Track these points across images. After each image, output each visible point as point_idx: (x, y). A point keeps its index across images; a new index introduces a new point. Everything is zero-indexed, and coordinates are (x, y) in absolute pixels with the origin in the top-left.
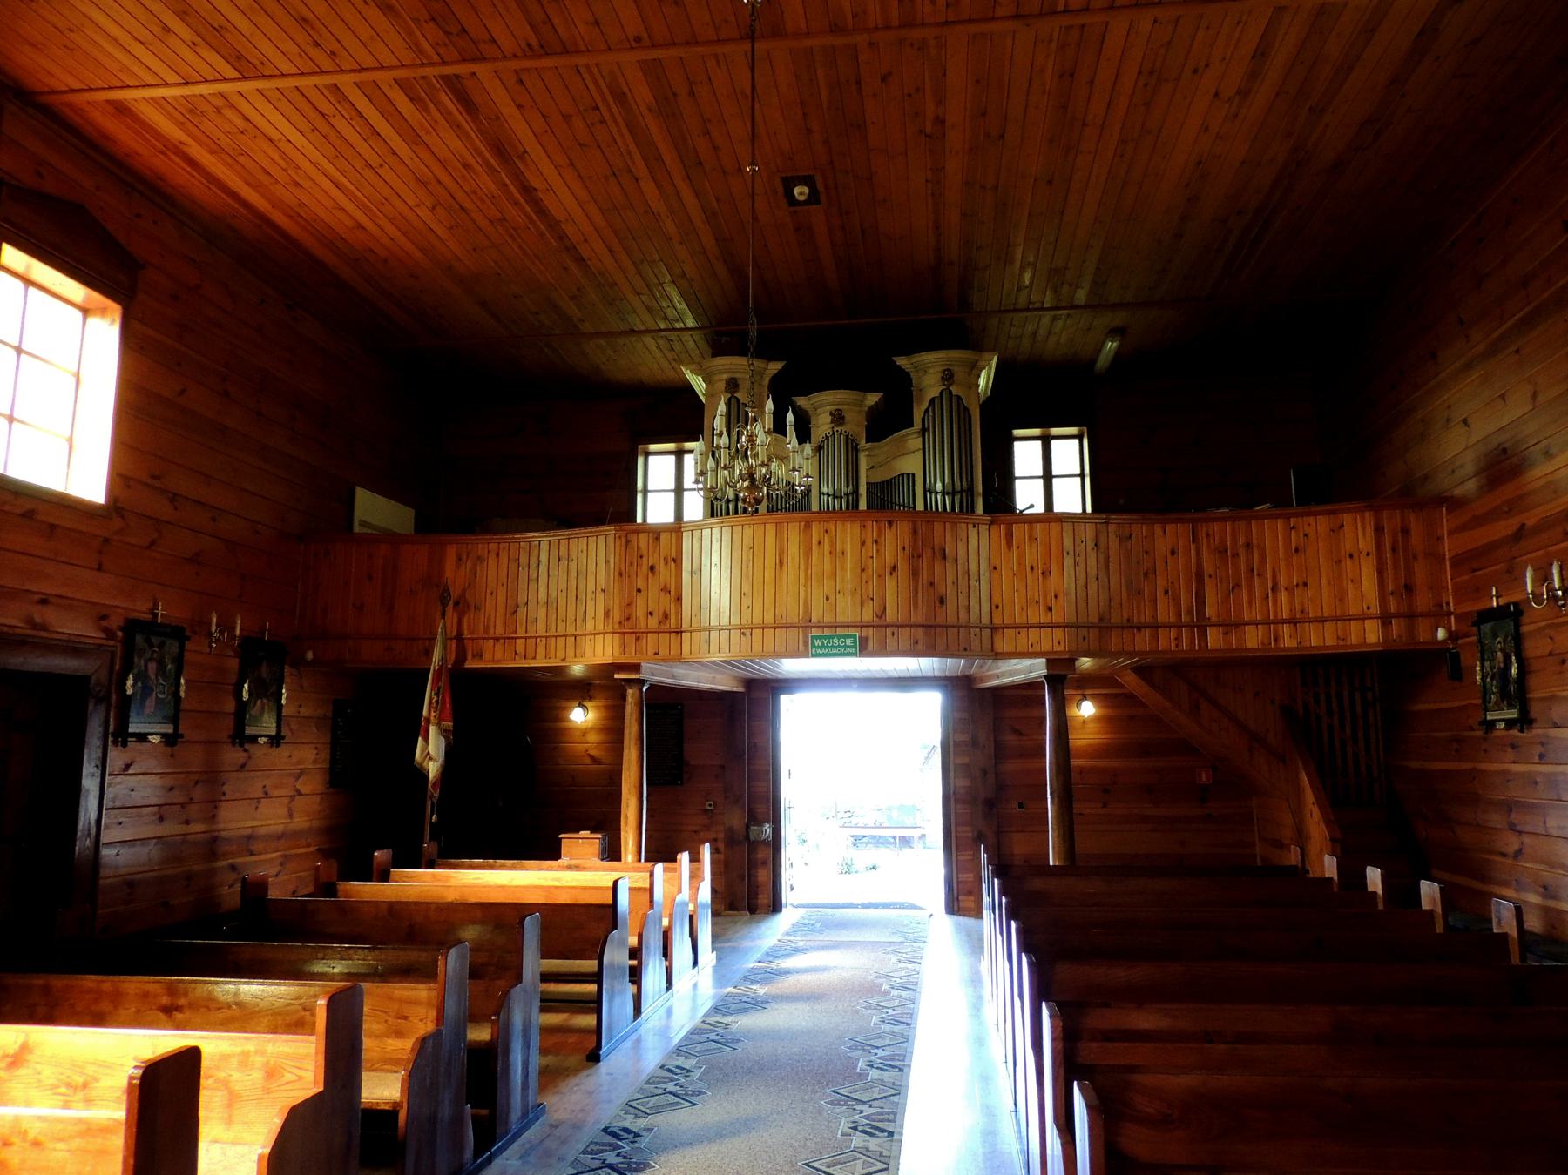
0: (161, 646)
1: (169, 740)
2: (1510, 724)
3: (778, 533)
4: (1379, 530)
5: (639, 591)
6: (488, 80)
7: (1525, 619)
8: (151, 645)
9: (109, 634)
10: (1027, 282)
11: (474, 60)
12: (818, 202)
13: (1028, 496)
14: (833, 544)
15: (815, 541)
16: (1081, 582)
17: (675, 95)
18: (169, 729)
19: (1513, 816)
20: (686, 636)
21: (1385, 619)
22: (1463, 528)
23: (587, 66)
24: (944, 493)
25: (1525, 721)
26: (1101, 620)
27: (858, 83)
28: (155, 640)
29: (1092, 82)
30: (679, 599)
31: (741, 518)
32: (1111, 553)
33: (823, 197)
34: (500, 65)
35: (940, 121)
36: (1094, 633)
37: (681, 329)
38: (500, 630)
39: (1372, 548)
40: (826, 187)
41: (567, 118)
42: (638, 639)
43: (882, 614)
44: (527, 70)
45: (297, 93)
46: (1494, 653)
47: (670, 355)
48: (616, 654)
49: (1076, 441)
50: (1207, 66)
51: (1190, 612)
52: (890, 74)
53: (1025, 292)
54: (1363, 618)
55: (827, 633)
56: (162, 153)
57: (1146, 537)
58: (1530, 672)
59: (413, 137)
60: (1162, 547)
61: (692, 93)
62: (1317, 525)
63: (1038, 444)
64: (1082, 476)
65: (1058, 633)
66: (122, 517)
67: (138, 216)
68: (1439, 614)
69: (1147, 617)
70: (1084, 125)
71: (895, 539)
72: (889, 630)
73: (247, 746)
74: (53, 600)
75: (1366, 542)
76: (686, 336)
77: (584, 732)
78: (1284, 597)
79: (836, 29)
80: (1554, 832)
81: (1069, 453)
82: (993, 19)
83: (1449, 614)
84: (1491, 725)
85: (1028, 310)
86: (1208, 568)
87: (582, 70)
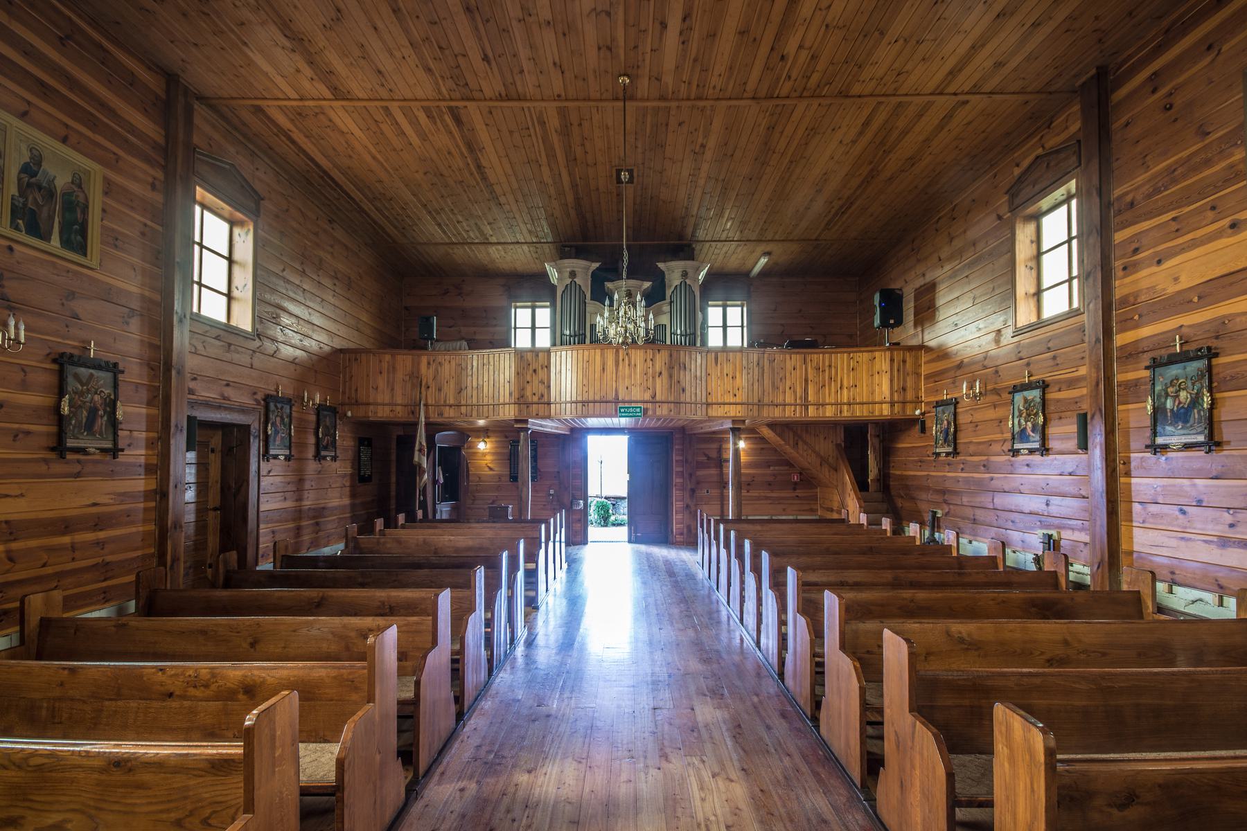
0: (282, 408)
1: (288, 458)
2: (948, 454)
3: (602, 355)
4: (892, 360)
5: (528, 382)
6: (473, 112)
7: (959, 406)
8: (277, 409)
9: (258, 403)
10: (728, 227)
11: (468, 99)
12: (632, 182)
13: (714, 339)
14: (630, 361)
15: (621, 359)
16: (751, 383)
17: (571, 124)
18: (287, 452)
19: (946, 496)
20: (553, 406)
21: (892, 404)
22: (932, 361)
23: (529, 108)
24: (681, 335)
25: (956, 452)
26: (759, 401)
27: (667, 125)
28: (279, 406)
29: (782, 132)
30: (549, 387)
31: (577, 346)
32: (765, 368)
33: (635, 180)
34: (482, 104)
35: (703, 146)
36: (756, 407)
37: (544, 243)
38: (452, 402)
39: (888, 369)
40: (638, 176)
41: (511, 132)
42: (528, 407)
43: (654, 396)
44: (496, 107)
45: (364, 110)
46: (942, 421)
47: (534, 255)
48: (516, 414)
49: (740, 309)
50: (840, 127)
51: (801, 398)
52: (684, 122)
53: (726, 232)
54: (881, 403)
55: (627, 405)
56: (277, 135)
57: (11, 249)
58: (960, 431)
59: (424, 137)
60: (789, 365)
61: (580, 125)
62: (863, 357)
63: (721, 309)
64: (742, 326)
65: (739, 407)
66: (260, 339)
67: (257, 169)
68: (917, 402)
69: (780, 400)
70: (774, 152)
71: (661, 359)
72: (657, 405)
73: (322, 462)
74: (231, 384)
75: (885, 366)
76: (546, 246)
77: (484, 454)
78: (845, 391)
79: (662, 98)
80: (964, 503)
81: (735, 314)
82: (742, 99)
83: (922, 402)
84: (938, 454)
85: (726, 241)
86: (810, 377)
87: (526, 110)
